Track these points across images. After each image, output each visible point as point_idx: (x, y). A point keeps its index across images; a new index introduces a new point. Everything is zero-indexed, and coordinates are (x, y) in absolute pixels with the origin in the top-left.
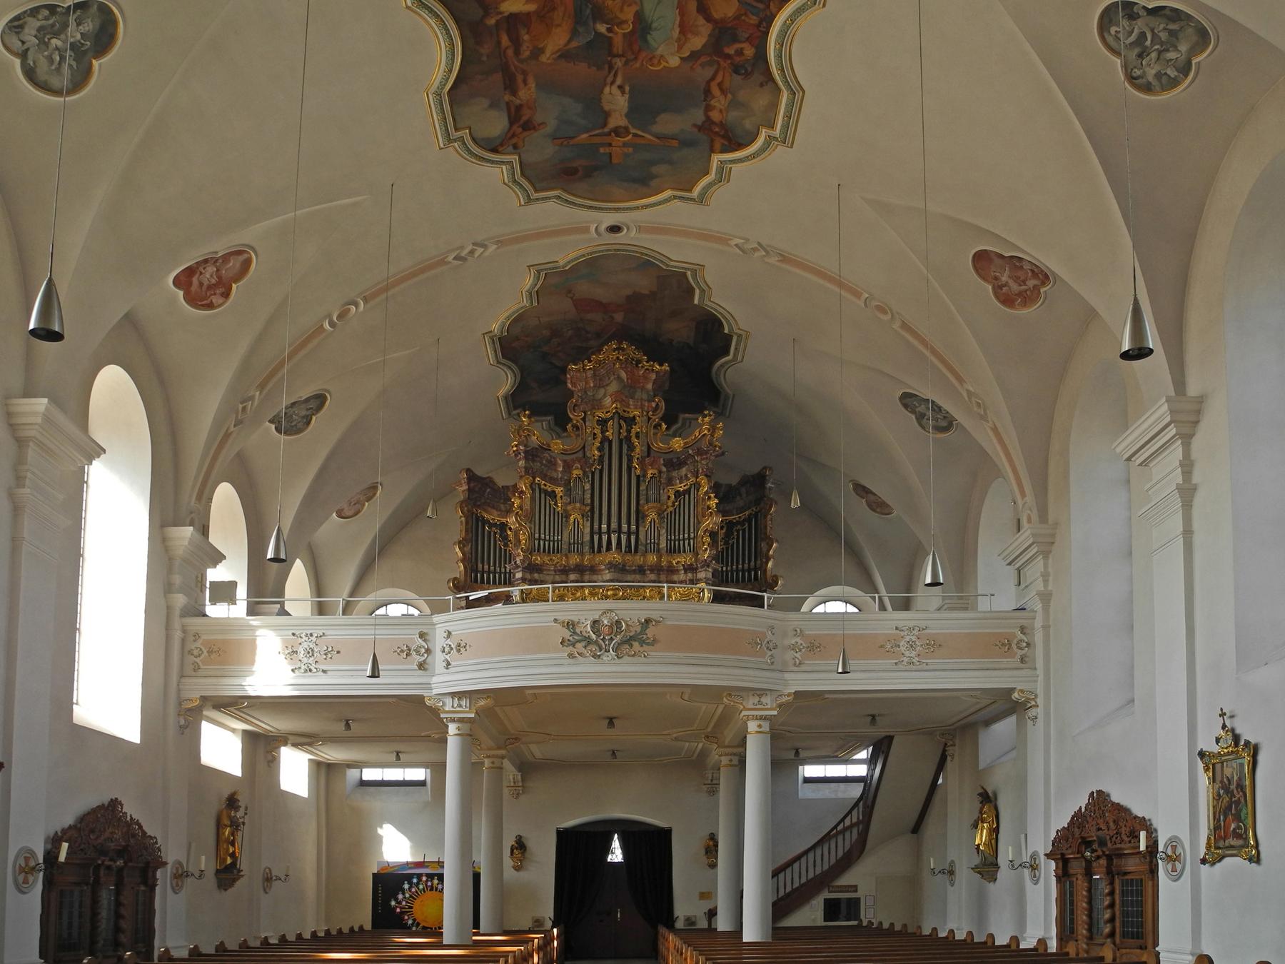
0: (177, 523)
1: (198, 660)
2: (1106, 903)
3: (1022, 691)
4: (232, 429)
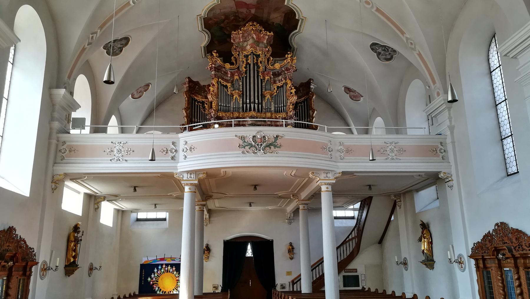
0: (58, 87)
1: (64, 155)
2: (517, 284)
3: (445, 173)
4: (86, 46)
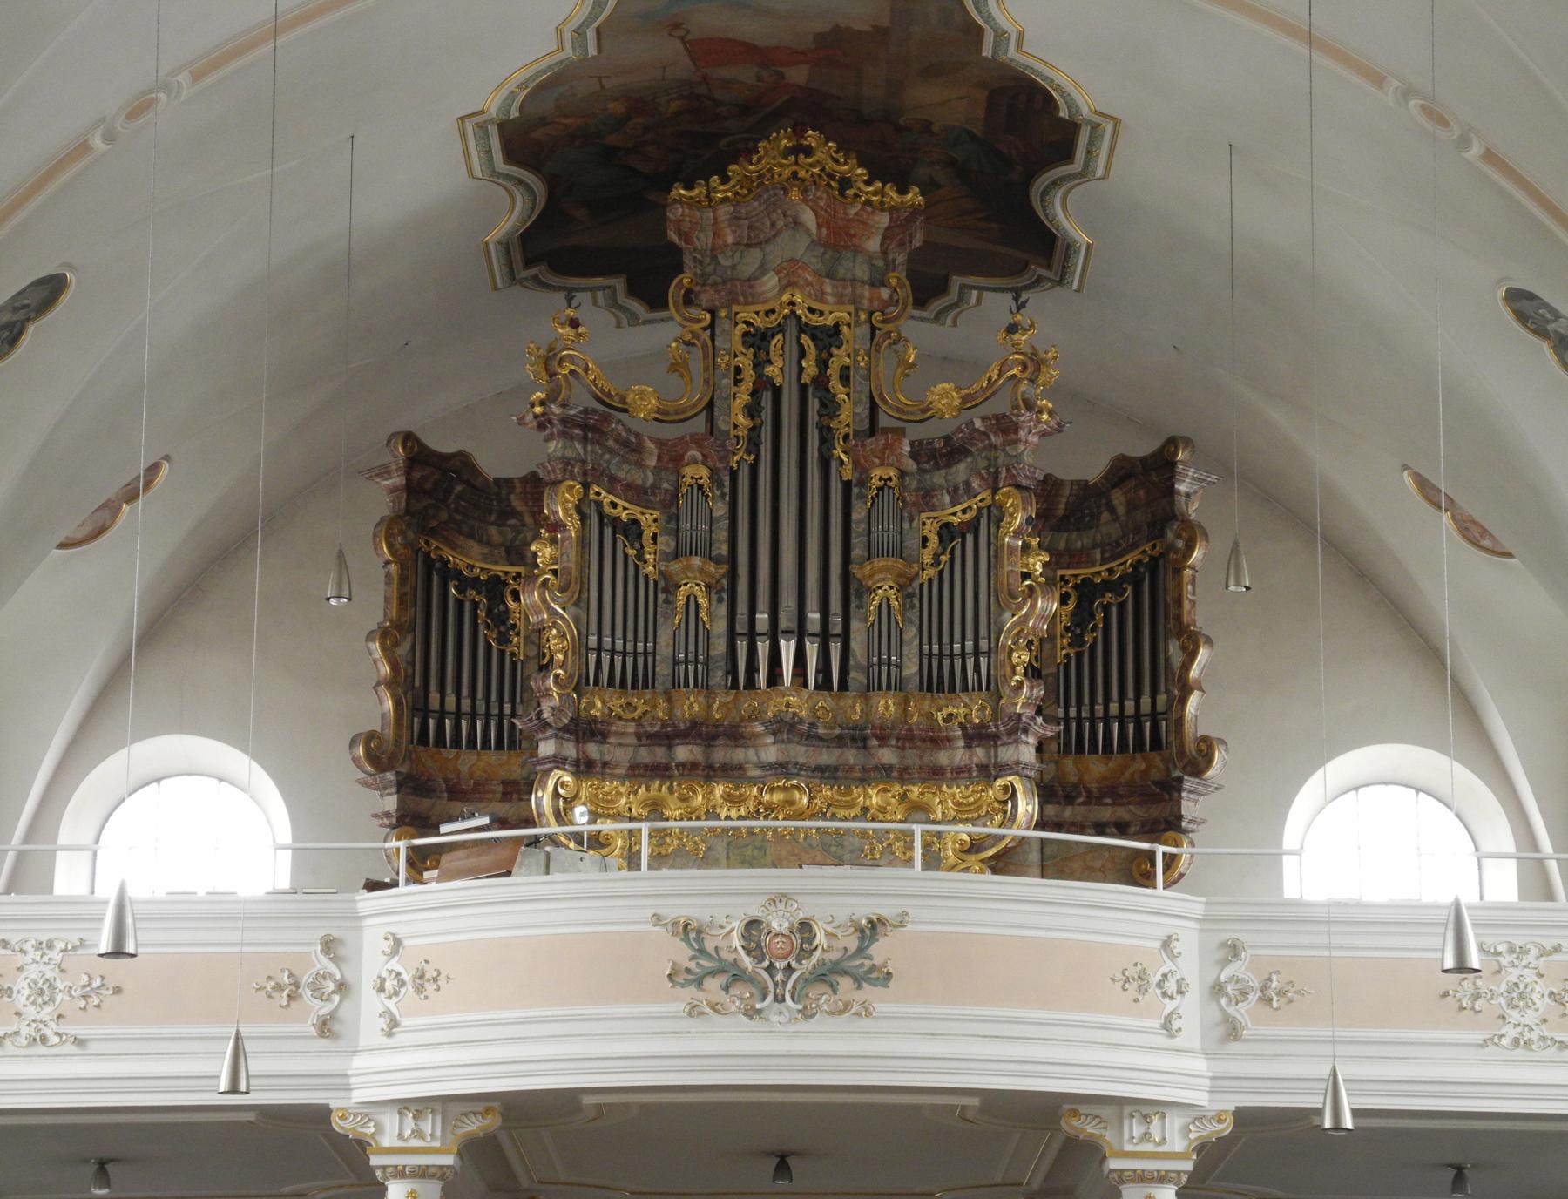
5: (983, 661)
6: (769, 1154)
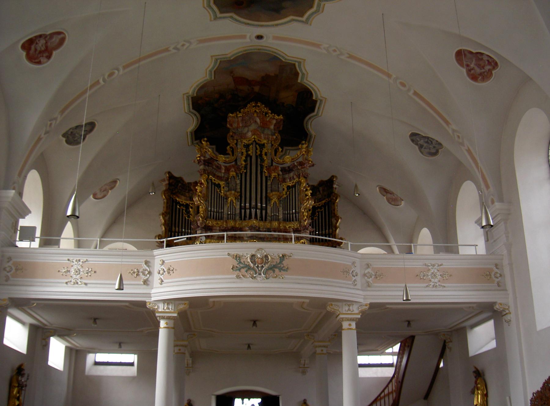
0: (6, 188)
1: (9, 274)
3: (501, 304)
4: (43, 135)
5: (297, 215)
6: (251, 321)
